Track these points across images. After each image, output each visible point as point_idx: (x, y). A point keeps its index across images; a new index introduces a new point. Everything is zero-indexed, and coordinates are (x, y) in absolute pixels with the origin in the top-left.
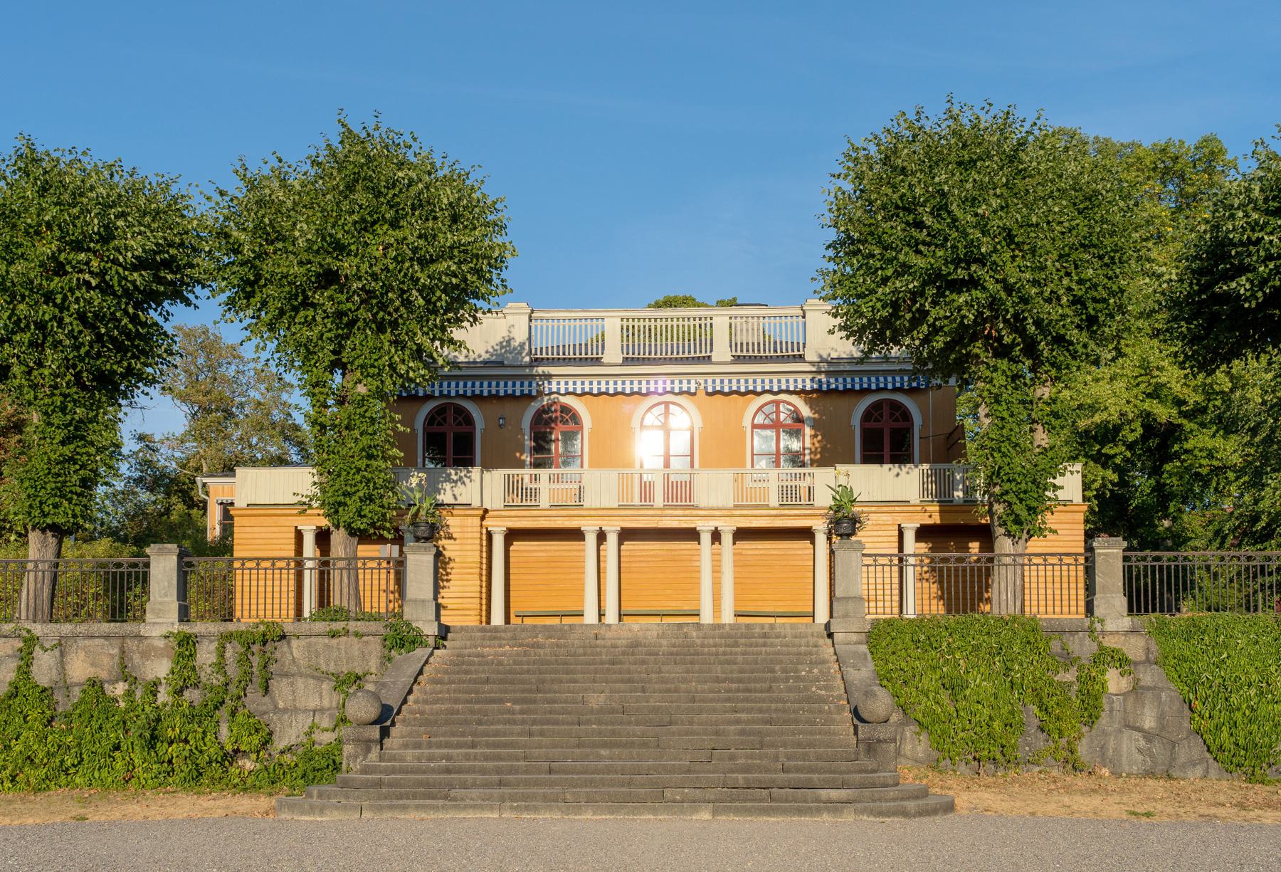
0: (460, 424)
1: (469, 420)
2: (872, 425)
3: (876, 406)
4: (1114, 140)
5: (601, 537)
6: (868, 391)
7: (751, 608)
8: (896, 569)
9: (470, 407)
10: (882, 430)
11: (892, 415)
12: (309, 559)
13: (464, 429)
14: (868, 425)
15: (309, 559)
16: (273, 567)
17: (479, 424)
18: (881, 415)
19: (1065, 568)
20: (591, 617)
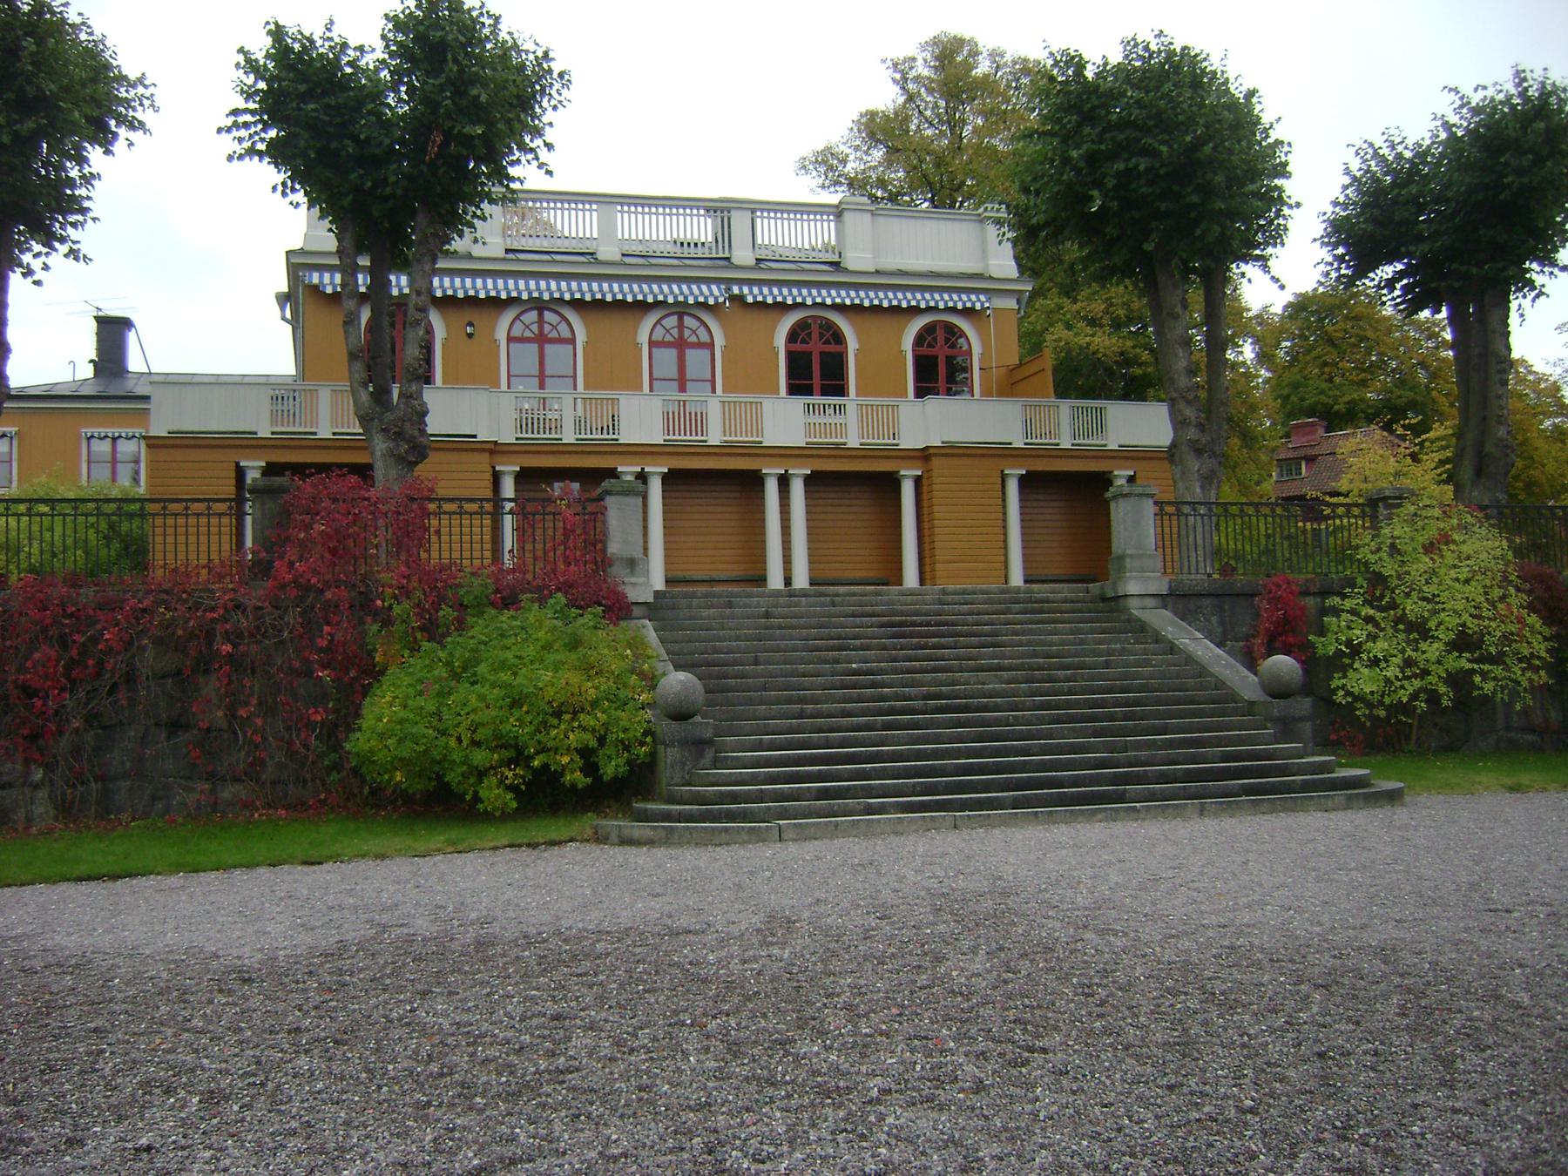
0: (827, 342)
1: (838, 338)
2: (925, 350)
3: (929, 330)
4: (986, 43)
5: (784, 482)
6: (803, 305)
7: (680, 574)
8: (487, 522)
9: (962, 324)
10: (936, 357)
11: (821, 336)
12: (510, 500)
13: (832, 348)
14: (794, 347)
15: (510, 500)
16: (1179, 513)
17: (852, 344)
18: (935, 339)
19: (214, 520)
20: (775, 581)
